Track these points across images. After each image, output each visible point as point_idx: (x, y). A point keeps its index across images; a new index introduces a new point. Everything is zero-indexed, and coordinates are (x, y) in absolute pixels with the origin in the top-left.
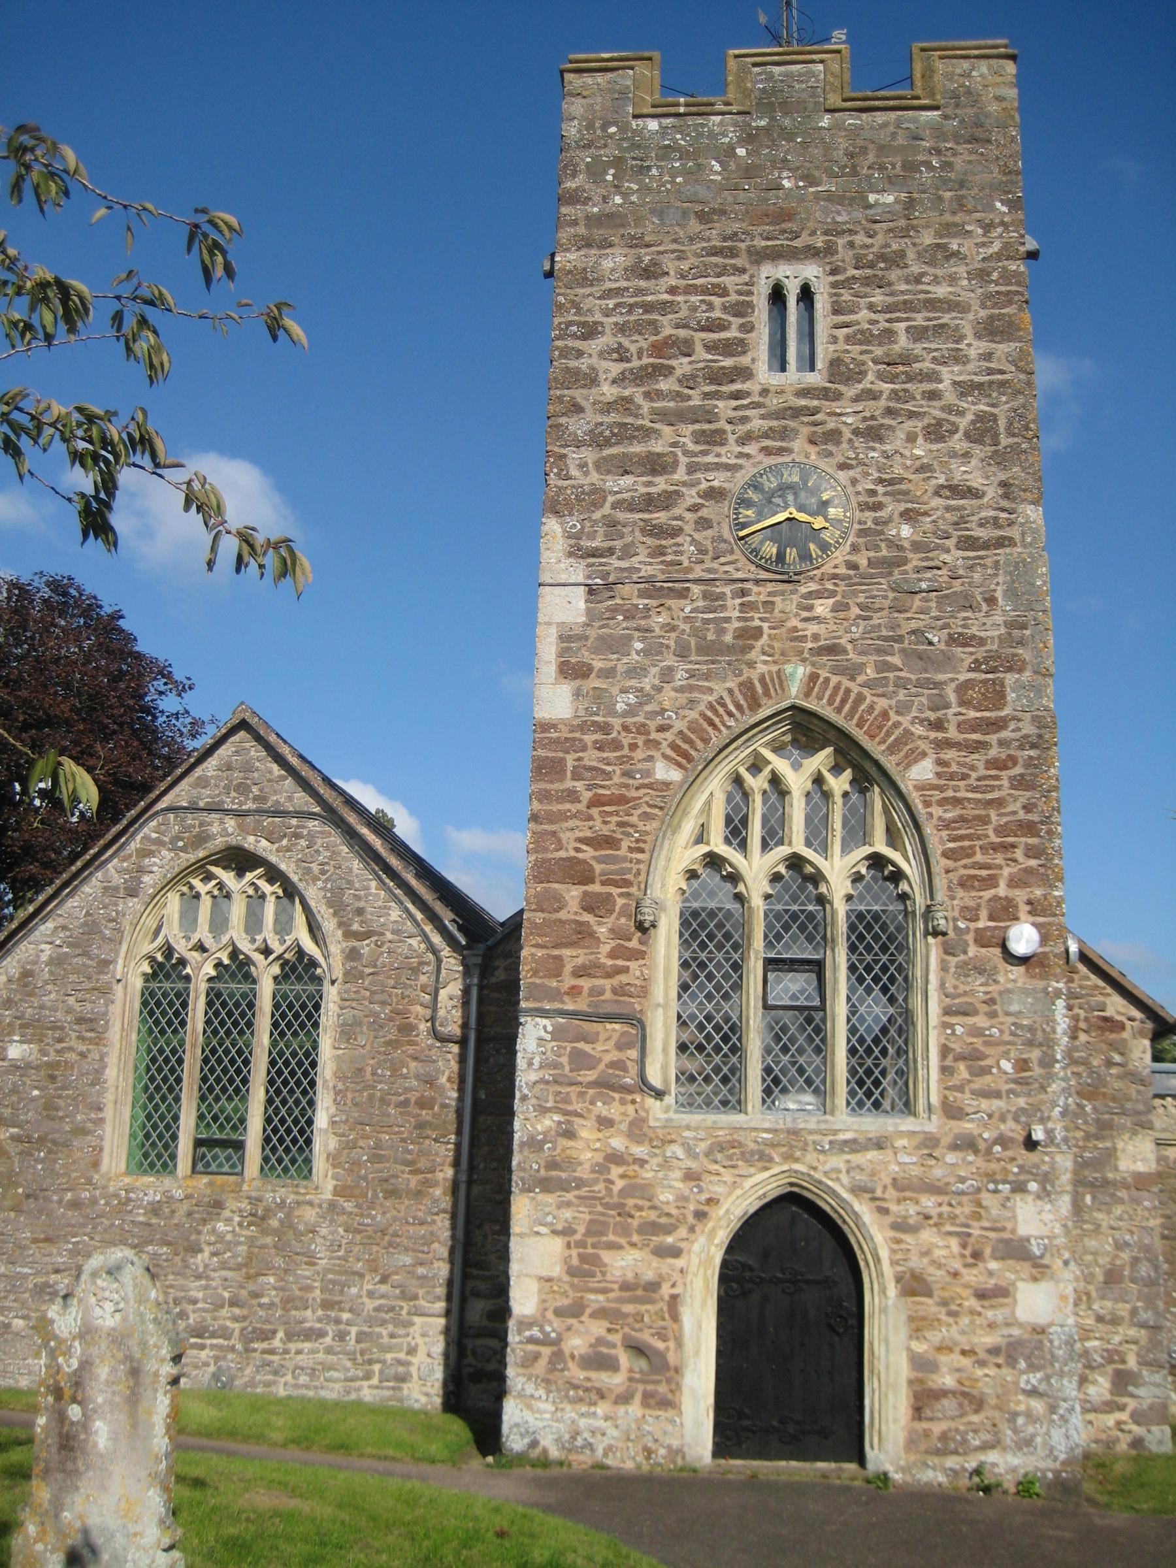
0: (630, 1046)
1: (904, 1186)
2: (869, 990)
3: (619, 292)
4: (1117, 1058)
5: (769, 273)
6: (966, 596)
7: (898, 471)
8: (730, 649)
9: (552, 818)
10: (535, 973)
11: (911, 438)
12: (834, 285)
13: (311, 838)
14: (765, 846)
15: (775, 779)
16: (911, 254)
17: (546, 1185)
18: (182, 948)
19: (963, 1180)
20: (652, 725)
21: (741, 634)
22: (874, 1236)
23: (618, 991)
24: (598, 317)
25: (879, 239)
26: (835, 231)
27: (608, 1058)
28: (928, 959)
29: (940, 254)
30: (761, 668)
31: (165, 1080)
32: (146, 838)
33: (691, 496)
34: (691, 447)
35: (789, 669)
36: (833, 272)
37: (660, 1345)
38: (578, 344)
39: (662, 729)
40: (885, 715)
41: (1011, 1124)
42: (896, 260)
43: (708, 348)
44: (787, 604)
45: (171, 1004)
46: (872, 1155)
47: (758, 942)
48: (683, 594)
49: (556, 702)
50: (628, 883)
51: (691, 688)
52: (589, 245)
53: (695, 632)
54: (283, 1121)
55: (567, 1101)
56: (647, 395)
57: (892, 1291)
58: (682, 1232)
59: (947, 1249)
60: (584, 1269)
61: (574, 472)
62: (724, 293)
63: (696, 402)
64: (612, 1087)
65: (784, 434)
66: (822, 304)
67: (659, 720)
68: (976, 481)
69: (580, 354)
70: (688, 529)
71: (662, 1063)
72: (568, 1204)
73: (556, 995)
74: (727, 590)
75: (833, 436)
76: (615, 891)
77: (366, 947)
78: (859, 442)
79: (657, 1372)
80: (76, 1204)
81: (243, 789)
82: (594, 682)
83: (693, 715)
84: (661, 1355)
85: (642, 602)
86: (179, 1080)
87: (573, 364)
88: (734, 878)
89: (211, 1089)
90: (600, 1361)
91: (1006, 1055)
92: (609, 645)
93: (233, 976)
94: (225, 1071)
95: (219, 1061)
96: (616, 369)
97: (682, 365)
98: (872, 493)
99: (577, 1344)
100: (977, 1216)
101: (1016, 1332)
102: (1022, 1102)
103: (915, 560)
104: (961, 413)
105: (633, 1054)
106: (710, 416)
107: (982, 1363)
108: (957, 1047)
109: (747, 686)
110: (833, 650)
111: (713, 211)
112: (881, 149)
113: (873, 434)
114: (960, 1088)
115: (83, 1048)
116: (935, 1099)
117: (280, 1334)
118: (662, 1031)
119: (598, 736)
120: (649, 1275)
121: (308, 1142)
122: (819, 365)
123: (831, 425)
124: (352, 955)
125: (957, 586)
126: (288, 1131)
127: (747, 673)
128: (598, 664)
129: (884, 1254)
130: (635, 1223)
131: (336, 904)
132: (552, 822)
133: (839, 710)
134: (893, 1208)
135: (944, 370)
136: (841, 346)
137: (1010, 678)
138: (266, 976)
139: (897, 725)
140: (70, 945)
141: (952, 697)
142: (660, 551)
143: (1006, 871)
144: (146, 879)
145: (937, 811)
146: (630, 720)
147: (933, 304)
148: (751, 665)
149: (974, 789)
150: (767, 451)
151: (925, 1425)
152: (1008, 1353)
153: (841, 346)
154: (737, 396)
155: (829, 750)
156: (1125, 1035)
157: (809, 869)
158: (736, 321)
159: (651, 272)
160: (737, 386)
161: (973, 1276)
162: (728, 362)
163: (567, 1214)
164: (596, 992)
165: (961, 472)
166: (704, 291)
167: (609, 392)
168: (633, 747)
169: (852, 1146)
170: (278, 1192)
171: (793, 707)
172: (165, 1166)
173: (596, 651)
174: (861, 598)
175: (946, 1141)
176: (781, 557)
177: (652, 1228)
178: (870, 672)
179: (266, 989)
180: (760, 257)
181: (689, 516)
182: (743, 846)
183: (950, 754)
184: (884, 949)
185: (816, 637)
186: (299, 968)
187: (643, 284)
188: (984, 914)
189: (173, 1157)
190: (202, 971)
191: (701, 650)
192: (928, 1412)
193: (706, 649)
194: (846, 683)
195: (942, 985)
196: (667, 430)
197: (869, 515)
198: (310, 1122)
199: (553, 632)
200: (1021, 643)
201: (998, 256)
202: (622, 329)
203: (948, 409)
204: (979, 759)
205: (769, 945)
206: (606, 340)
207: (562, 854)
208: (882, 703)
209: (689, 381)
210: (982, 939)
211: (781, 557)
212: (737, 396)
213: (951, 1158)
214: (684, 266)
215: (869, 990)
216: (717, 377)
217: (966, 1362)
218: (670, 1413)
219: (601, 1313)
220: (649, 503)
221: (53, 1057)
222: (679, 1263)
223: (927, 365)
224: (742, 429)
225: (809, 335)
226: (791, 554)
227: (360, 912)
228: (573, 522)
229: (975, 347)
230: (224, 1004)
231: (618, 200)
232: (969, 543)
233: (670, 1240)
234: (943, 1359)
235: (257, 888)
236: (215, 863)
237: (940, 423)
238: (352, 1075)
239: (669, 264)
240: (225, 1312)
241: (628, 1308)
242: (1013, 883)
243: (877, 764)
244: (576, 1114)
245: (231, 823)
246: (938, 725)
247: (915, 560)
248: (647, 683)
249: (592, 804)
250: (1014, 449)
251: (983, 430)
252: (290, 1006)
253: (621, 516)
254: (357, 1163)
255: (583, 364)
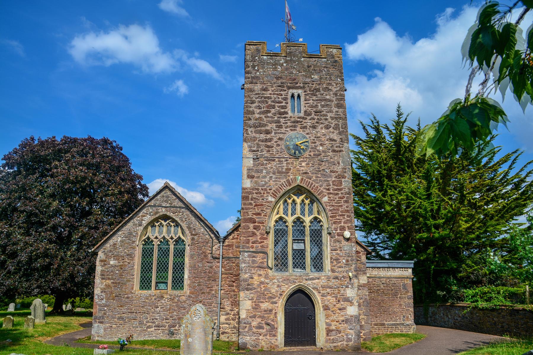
0: (265, 258)
1: (323, 287)
2: (314, 246)
3: (258, 94)
4: (359, 259)
5: (291, 91)
6: (333, 162)
7: (319, 135)
8: (284, 173)
9: (246, 209)
10: (244, 243)
11: (322, 128)
12: (305, 95)
13: (183, 212)
14: (292, 215)
15: (294, 201)
16: (321, 89)
17: (247, 289)
18: (152, 238)
19: (335, 285)
20: (268, 189)
21: (287, 169)
22: (318, 298)
23: (262, 247)
24: (254, 99)
25: (314, 86)
26: (305, 83)
27: (260, 261)
28: (326, 239)
29: (327, 89)
30: (291, 177)
31: (148, 268)
32: (143, 213)
33: (275, 139)
34: (275, 128)
35: (297, 177)
36: (305, 92)
37: (273, 323)
38: (250, 105)
39: (270, 190)
40: (317, 187)
41: (345, 273)
42: (318, 90)
43: (279, 107)
44: (296, 163)
45: (150, 251)
46: (317, 280)
47: (291, 236)
48: (274, 160)
49: (248, 184)
50: (263, 223)
51: (276, 181)
52: (252, 83)
53: (277, 169)
54: (177, 277)
55: (251, 271)
56: (265, 117)
57: (322, 309)
58: (277, 299)
59: (333, 300)
60: (256, 307)
61: (250, 133)
62: (282, 95)
63: (276, 119)
64: (261, 268)
65: (295, 126)
66: (302, 99)
67: (269, 188)
68: (335, 138)
69: (251, 107)
70: (275, 146)
71: (271, 262)
72: (252, 293)
73: (248, 248)
74: (283, 160)
75: (305, 127)
76: (261, 225)
77: (196, 237)
78: (311, 129)
79: (273, 329)
80: (128, 298)
81: (166, 201)
82: (255, 179)
83: (277, 187)
84: (273, 325)
85: (265, 162)
86: (152, 268)
87: (249, 109)
88: (285, 222)
89: (159, 270)
90: (260, 327)
91: (344, 259)
92: (257, 171)
93: (164, 244)
94: (163, 266)
95: (161, 264)
96: (258, 111)
97: (273, 111)
98: (314, 140)
99: (254, 324)
100: (339, 293)
101: (347, 317)
102: (347, 269)
103: (323, 154)
104: (332, 123)
105: (266, 260)
106: (279, 122)
107: (340, 324)
108: (334, 257)
109: (288, 181)
110: (306, 173)
111: (279, 77)
112: (315, 66)
113: (314, 127)
114: (334, 266)
115: (128, 261)
116: (329, 269)
117: (177, 326)
118: (271, 255)
119: (256, 191)
120: (270, 308)
121: (183, 282)
122: (302, 112)
123: (305, 125)
124: (193, 239)
125: (332, 160)
126: (178, 279)
127: (288, 178)
128: (256, 175)
129: (320, 302)
130: (267, 297)
131: (189, 228)
132: (246, 210)
133: (308, 186)
134: (321, 292)
135: (328, 114)
136: (307, 108)
137: (343, 180)
138: (156, 243)
139: (320, 189)
140: (125, 237)
141: (331, 184)
142: (269, 151)
143: (343, 220)
144: (143, 222)
145: (328, 208)
146: (263, 188)
147: (326, 100)
148: (289, 176)
149: (336, 203)
150: (291, 130)
151: (329, 337)
152: (346, 321)
153: (307, 108)
154: (285, 118)
155: (305, 195)
156: (361, 254)
157: (301, 220)
158: (284, 102)
159: (265, 90)
160: (284, 116)
161: (338, 306)
162: (283, 110)
163: (252, 295)
164: (257, 247)
165: (332, 136)
166: (277, 95)
167: (257, 116)
168: (264, 193)
169: (312, 279)
170: (177, 292)
171: (298, 185)
172: (149, 288)
173: (255, 172)
174: (312, 162)
175: (333, 277)
176: (295, 153)
177: (271, 298)
178: (314, 178)
179: (172, 247)
180: (289, 88)
181: (275, 143)
182: (287, 215)
183: (331, 196)
184: (317, 237)
185: (303, 170)
186: (179, 241)
187: (264, 92)
188: (338, 229)
189: (151, 286)
190: (156, 243)
191: (278, 173)
192: (330, 335)
193: (279, 172)
194: (309, 180)
195: (331, 244)
196: (269, 124)
197: (313, 144)
198: (183, 277)
199: (246, 169)
200: (345, 172)
201: (339, 91)
202: (259, 102)
203: (329, 122)
204: (337, 197)
205: (293, 236)
206: (256, 104)
207: (249, 217)
208: (317, 185)
209: (274, 114)
210: (338, 235)
211: (295, 153)
212: (285, 118)
213: (333, 281)
214: (273, 89)
215: (314, 246)
216: (281, 113)
217: (337, 324)
218: (276, 338)
219: (260, 317)
220: (266, 140)
221: (121, 263)
222: (277, 305)
223: (324, 113)
224: (286, 125)
225: (299, 105)
226: (297, 152)
227: (194, 229)
228: (249, 144)
229: (335, 109)
230: (162, 251)
231: (258, 73)
232: (334, 151)
233: (274, 300)
234: (333, 323)
235: (169, 224)
236: (160, 219)
237: (327, 125)
238: (193, 267)
239: (270, 89)
240: (164, 321)
241: (266, 316)
242: (344, 223)
243: (316, 197)
244: (253, 274)
245: (164, 210)
246: (328, 189)
247: (323, 154)
248: (266, 180)
249: (256, 205)
250: (343, 131)
251: (336, 127)
252: (178, 251)
253: (260, 143)
254: (195, 286)
255: (251, 109)
